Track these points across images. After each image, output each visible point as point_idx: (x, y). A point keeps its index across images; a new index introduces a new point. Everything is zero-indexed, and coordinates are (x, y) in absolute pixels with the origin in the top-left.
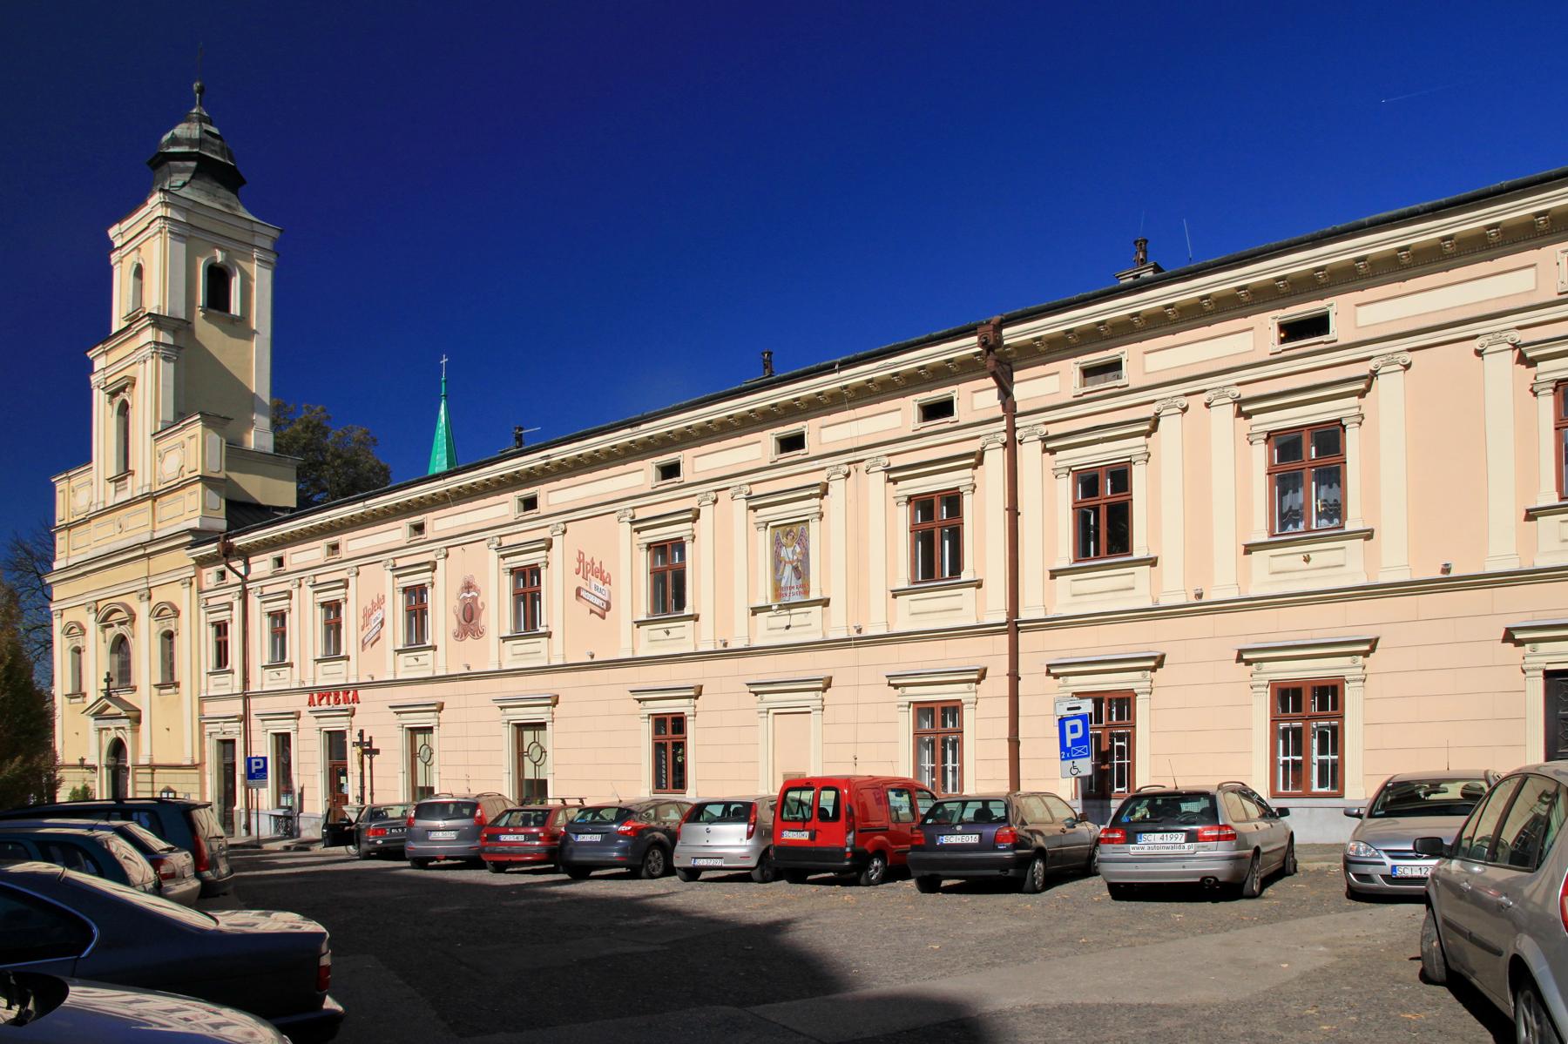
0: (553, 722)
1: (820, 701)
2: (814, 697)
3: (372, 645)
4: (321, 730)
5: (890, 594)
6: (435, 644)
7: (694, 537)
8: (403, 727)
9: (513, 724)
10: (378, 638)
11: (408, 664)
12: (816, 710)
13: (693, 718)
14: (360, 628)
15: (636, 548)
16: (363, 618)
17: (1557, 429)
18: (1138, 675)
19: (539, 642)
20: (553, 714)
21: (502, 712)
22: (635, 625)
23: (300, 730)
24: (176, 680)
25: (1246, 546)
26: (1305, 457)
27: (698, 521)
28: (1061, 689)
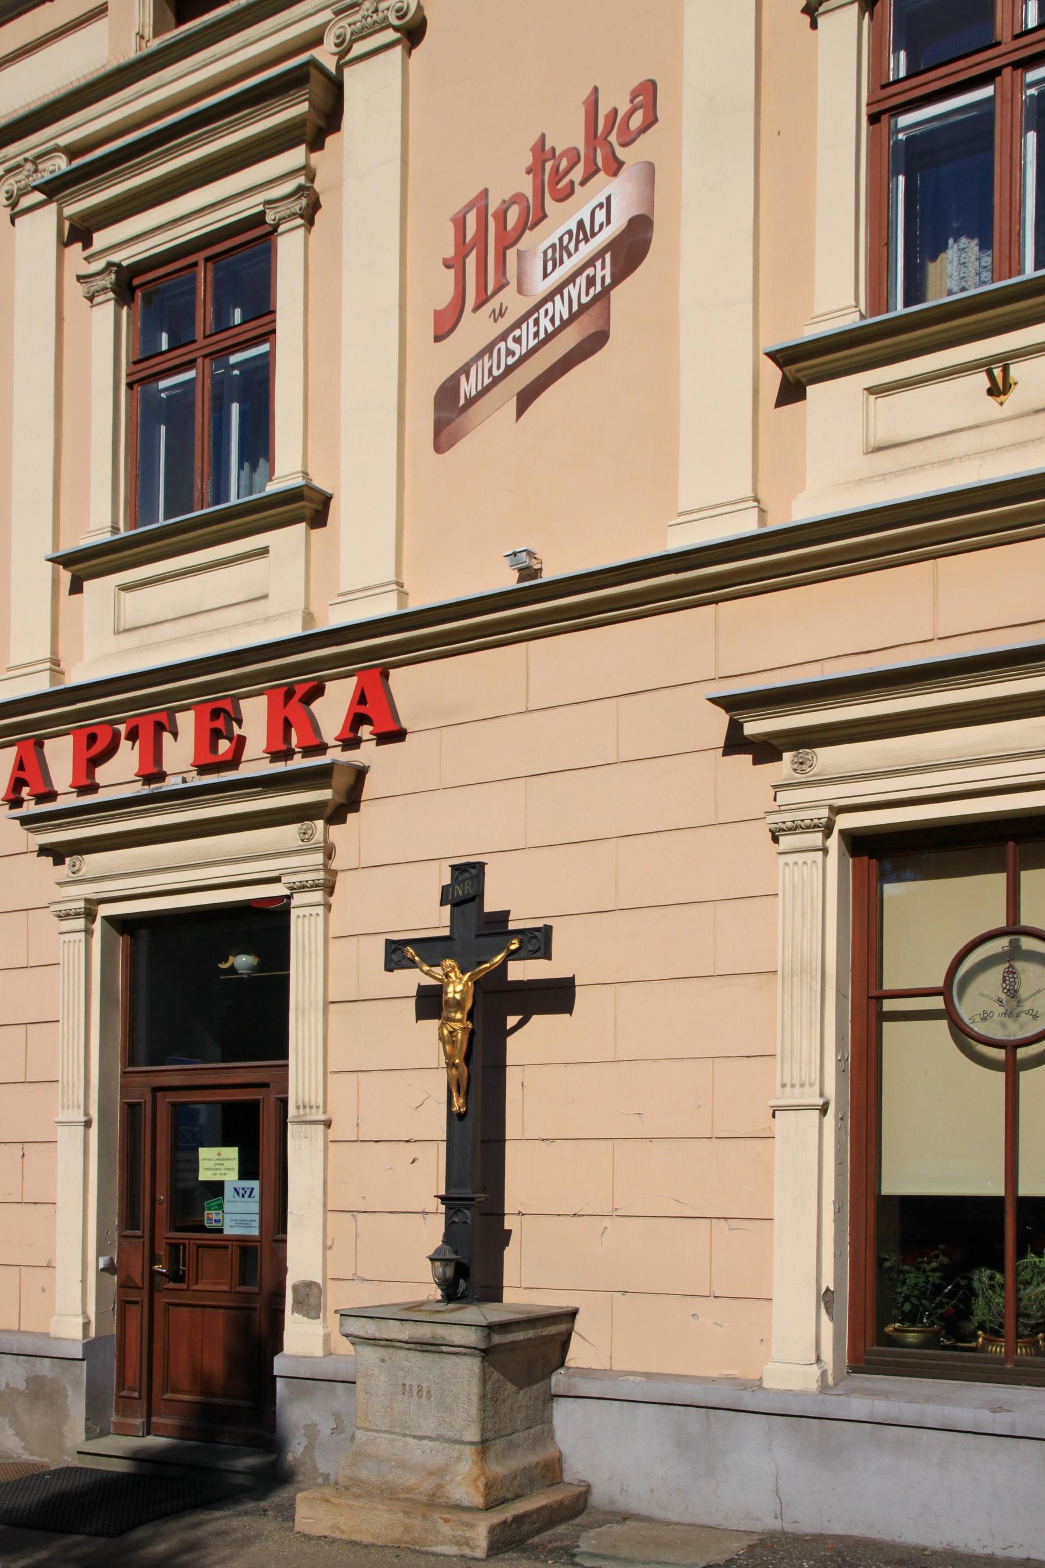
0: (329, 889)
1: (319, 858)
2: (297, 843)
3: (525, 399)
4: (90, 915)
5: (772, 376)
6: (321, 483)
7: (315, 205)
8: (90, 915)
9: (107, 919)
10: (597, 341)
11: (882, 434)
12: (303, 888)
13: (318, 896)
14: (422, 326)
15: (75, 291)
16: (456, 264)
17: (874, 119)
18: (288, 834)
19: (264, 551)
20: (329, 852)
21: (64, 871)
22: (66, 576)
23: (342, 883)
24: (87, 585)
25: (782, 357)
26: (1003, 31)
27: (330, 141)
28: (784, 797)
